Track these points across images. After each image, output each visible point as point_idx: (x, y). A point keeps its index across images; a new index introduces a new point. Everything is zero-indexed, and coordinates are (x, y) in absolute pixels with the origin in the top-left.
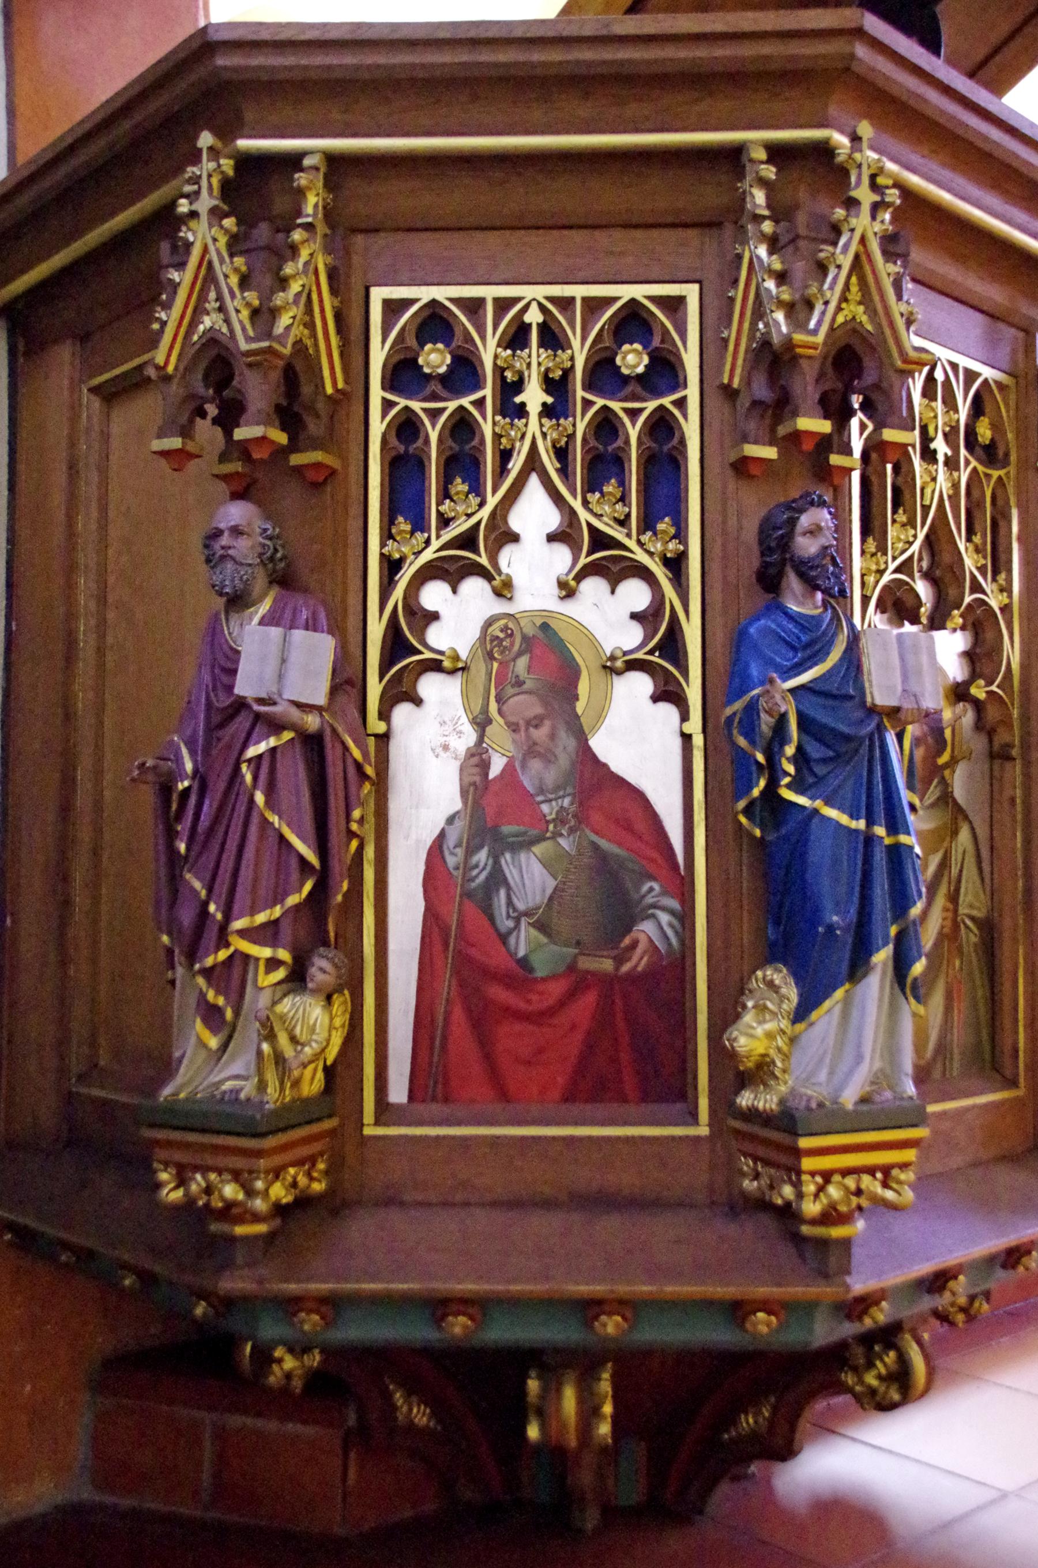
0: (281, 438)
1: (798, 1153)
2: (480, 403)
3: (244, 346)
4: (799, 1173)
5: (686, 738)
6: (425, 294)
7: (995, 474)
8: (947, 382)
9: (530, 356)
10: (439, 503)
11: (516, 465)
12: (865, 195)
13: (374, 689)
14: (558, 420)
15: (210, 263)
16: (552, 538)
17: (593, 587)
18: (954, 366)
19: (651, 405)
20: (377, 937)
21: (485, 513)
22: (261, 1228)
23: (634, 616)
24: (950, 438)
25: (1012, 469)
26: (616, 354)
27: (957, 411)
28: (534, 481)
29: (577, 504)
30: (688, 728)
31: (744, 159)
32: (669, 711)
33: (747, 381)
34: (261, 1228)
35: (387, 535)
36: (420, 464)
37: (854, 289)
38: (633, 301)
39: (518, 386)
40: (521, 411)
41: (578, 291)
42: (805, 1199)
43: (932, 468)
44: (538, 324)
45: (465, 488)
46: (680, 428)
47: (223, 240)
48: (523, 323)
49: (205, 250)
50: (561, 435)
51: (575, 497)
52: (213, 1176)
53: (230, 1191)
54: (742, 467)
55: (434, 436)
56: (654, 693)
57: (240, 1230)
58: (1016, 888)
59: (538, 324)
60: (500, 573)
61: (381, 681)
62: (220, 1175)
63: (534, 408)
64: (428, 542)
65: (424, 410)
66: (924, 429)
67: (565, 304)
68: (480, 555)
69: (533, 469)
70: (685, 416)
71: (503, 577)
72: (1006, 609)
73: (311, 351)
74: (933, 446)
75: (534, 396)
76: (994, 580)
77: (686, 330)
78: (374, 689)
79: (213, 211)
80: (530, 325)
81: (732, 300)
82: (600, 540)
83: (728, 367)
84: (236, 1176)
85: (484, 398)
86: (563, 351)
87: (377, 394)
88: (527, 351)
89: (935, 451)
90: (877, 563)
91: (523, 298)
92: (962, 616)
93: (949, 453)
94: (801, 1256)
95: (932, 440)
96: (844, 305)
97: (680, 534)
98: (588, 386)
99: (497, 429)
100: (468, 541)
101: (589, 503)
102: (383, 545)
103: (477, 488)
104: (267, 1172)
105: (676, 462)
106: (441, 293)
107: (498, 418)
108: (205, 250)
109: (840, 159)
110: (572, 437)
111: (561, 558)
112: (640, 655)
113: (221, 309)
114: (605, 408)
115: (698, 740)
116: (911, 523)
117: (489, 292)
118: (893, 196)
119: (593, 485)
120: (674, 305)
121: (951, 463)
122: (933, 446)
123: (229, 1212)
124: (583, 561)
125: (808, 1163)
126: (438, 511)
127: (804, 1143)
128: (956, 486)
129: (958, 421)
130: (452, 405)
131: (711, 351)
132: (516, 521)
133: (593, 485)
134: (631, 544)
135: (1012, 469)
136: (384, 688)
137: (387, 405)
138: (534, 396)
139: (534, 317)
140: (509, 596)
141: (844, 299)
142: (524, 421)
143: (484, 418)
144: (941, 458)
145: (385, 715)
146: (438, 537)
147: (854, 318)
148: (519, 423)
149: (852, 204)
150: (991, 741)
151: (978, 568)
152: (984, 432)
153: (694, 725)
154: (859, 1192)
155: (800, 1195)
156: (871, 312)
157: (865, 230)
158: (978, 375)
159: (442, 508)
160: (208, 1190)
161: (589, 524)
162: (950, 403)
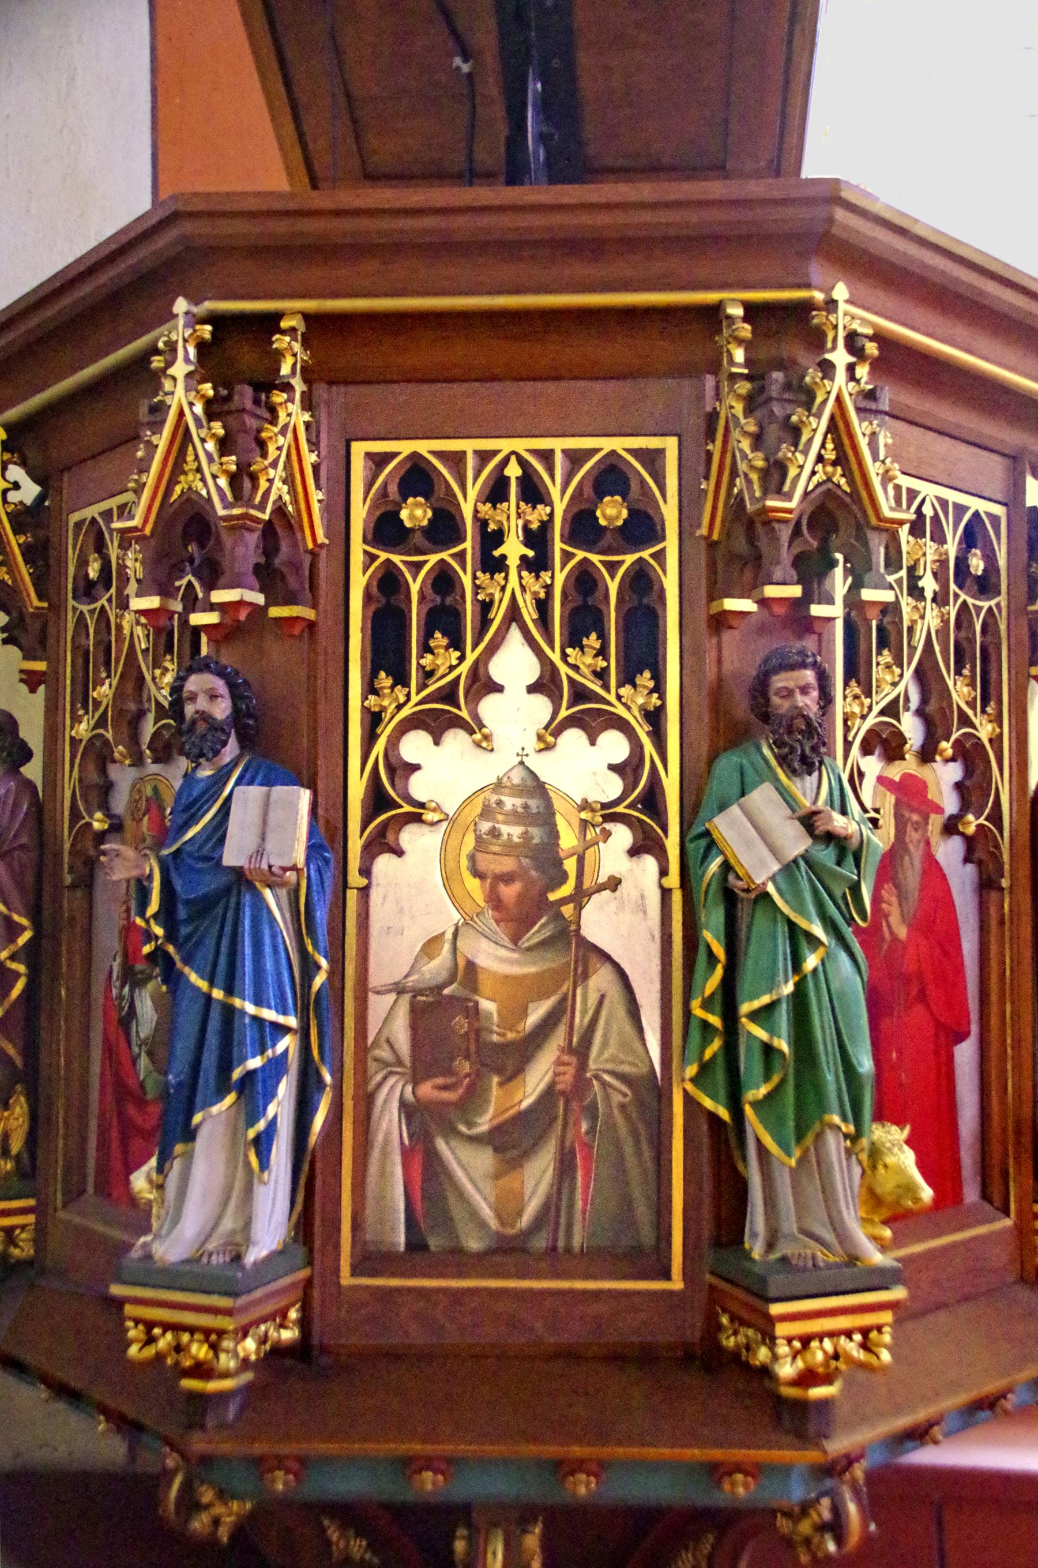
0: (259, 599)
2: (461, 557)
3: (221, 512)
5: (666, 893)
6: (405, 448)
7: (985, 605)
8: (936, 519)
10: (420, 656)
11: (498, 615)
12: (840, 357)
15: (187, 430)
16: (532, 689)
17: (574, 737)
18: (944, 503)
19: (629, 559)
21: (464, 669)
23: (612, 768)
25: (1002, 599)
29: (555, 657)
31: (722, 316)
33: (727, 534)
35: (370, 688)
38: (613, 453)
39: (498, 538)
41: (558, 445)
42: (781, 1361)
43: (921, 605)
44: (517, 478)
45: (445, 642)
46: (661, 582)
47: (199, 409)
49: (181, 414)
51: (553, 648)
53: (200, 1351)
54: (720, 622)
56: (632, 848)
58: (1012, 1003)
63: (513, 562)
65: (405, 563)
66: (912, 570)
72: (996, 741)
73: (290, 508)
74: (921, 584)
75: (513, 549)
76: (983, 711)
77: (665, 484)
78: (356, 844)
79: (189, 376)
81: (709, 455)
82: (580, 694)
89: (922, 589)
90: (862, 705)
91: (499, 451)
94: (779, 1417)
95: (920, 578)
97: (659, 688)
100: (449, 694)
102: (365, 698)
103: (456, 643)
106: (423, 447)
108: (181, 414)
109: (351, 1533)
110: (549, 588)
111: (541, 707)
112: (620, 809)
113: (199, 470)
114: (585, 560)
116: (899, 663)
117: (468, 446)
118: (872, 349)
120: (652, 459)
121: (940, 599)
122: (921, 584)
123: (202, 1370)
124: (564, 713)
125: (782, 1329)
126: (418, 664)
127: (776, 1309)
128: (946, 622)
130: (433, 559)
132: (498, 669)
133: (574, 639)
134: (612, 698)
135: (1002, 599)
138: (513, 549)
139: (513, 471)
140: (490, 748)
141: (820, 459)
142: (503, 575)
143: (465, 572)
144: (929, 594)
145: (366, 871)
148: (499, 577)
149: (827, 369)
150: (928, 1006)
151: (967, 703)
152: (977, 564)
154: (836, 1356)
157: (840, 389)
158: (967, 508)
159: (423, 662)
161: (569, 677)
162: (939, 538)
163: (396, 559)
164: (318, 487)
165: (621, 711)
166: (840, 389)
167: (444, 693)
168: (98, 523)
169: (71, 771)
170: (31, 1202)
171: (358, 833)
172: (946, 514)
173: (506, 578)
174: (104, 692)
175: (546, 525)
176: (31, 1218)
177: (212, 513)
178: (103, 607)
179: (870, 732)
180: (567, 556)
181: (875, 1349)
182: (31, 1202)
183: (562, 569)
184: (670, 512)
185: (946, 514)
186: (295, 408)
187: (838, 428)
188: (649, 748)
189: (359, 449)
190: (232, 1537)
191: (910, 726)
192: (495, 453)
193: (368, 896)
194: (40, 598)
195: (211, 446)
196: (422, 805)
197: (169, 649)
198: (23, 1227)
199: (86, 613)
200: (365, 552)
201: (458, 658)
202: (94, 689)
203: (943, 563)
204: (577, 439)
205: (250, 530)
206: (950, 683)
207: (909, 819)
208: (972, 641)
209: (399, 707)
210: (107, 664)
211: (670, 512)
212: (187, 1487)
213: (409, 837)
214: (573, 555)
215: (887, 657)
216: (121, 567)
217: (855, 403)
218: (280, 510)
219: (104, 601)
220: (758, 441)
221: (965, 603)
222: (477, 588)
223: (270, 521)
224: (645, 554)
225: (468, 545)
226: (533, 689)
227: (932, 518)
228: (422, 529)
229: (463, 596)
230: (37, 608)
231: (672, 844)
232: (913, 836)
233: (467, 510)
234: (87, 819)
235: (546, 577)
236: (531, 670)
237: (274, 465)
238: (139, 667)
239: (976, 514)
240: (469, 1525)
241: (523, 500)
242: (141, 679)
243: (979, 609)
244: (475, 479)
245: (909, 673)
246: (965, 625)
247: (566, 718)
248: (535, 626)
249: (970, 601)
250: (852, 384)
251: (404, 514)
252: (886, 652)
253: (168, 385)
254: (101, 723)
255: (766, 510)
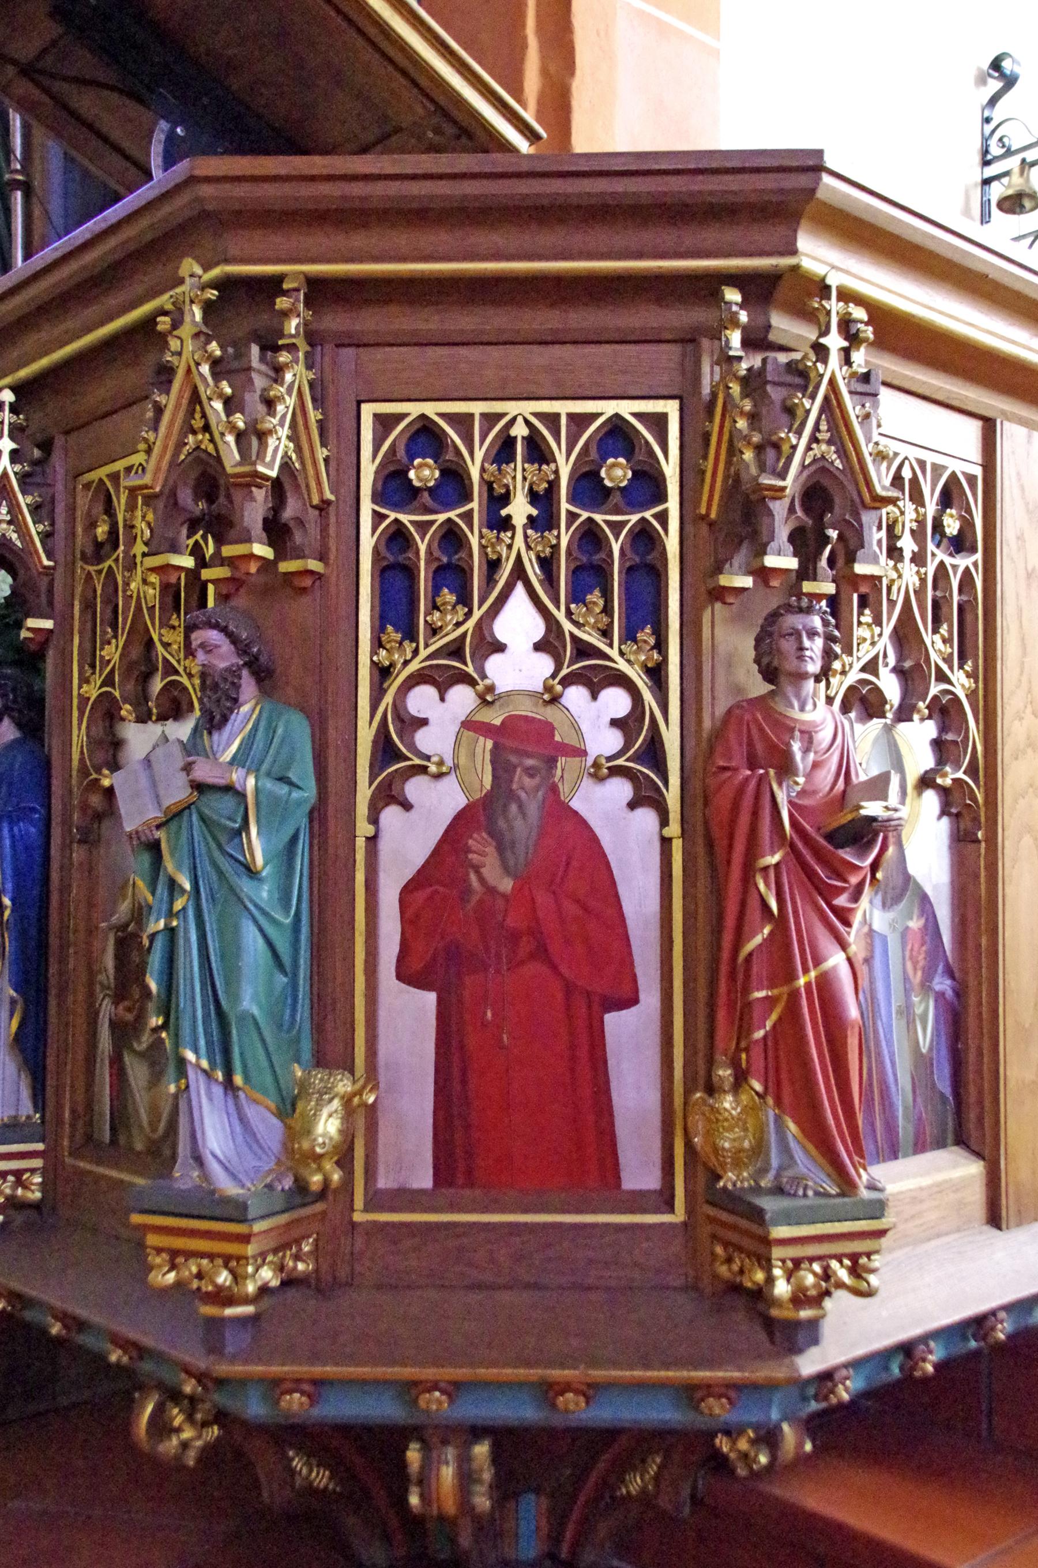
1: (767, 1242)
2: (468, 516)
4: (769, 1260)
5: (666, 842)
8: (915, 481)
9: (515, 470)
13: (364, 792)
14: (542, 533)
18: (922, 464)
20: (367, 1041)
21: (470, 624)
22: (249, 1309)
24: (918, 535)
26: (601, 467)
27: (923, 505)
28: (520, 589)
29: (560, 616)
30: (667, 832)
32: (646, 818)
34: (249, 1309)
35: (378, 644)
36: (410, 573)
37: (824, 427)
39: (505, 499)
40: (505, 524)
41: (563, 408)
44: (523, 438)
48: (509, 436)
50: (541, 480)
51: (558, 608)
52: (205, 1262)
53: (223, 1278)
55: (423, 548)
57: (229, 1312)
59: (523, 438)
60: (484, 676)
61: (370, 785)
62: (212, 1261)
64: (416, 652)
67: (552, 420)
68: (465, 664)
69: (518, 579)
70: (666, 530)
71: (487, 682)
73: (297, 465)
74: (899, 544)
75: (520, 509)
78: (364, 792)
80: (516, 437)
82: (583, 650)
83: (705, 497)
84: (227, 1260)
85: (472, 510)
86: (548, 464)
87: (367, 508)
88: (512, 465)
89: (901, 549)
92: (928, 707)
93: (916, 549)
95: (899, 538)
96: (814, 446)
97: (661, 645)
98: (572, 499)
99: (483, 541)
100: (455, 650)
101: (572, 614)
102: (374, 652)
103: (464, 599)
104: (255, 1257)
105: (657, 574)
107: (485, 531)
110: (556, 548)
112: (621, 762)
114: (590, 520)
115: (677, 846)
116: (878, 621)
117: (477, 408)
119: (577, 596)
121: (919, 559)
123: (223, 1297)
125: (777, 1252)
126: (426, 621)
128: (923, 581)
129: (925, 515)
130: (441, 517)
131: (690, 475)
132: (503, 628)
134: (614, 653)
136: (373, 793)
137: (378, 517)
138: (520, 509)
139: (520, 431)
141: (814, 439)
142: (509, 534)
143: (472, 533)
144: (907, 555)
145: (374, 819)
146: (427, 646)
147: (823, 457)
148: (506, 536)
153: (674, 829)
155: (770, 1280)
156: (842, 453)
158: (945, 468)
160: (200, 1276)
162: (917, 498)
163: (404, 518)
164: (324, 444)
165: (622, 665)
166: (833, 374)
167: (452, 648)
168: (105, 484)
169: (80, 729)
170: (40, 1146)
171: (367, 784)
172: (924, 472)
173: (512, 538)
174: (112, 652)
175: (553, 485)
176: (37, 1163)
177: (219, 469)
178: (110, 567)
179: (851, 689)
180: (572, 516)
181: (864, 1275)
182: (40, 1146)
183: (568, 529)
184: (671, 470)
185: (924, 472)
186: (300, 368)
187: (832, 406)
188: (648, 696)
189: (368, 411)
190: (199, 1460)
191: (890, 687)
192: (502, 416)
193: (375, 845)
194: (49, 558)
195: (218, 405)
196: (428, 758)
197: (177, 608)
198: (33, 1171)
199: (93, 573)
200: (374, 511)
201: (465, 614)
202: (102, 649)
203: (921, 522)
204: (678, 703)
205: (260, 487)
206: (928, 641)
207: (520, 764)
208: (949, 601)
209: (406, 663)
210: (114, 626)
211: (671, 470)
212: (160, 1410)
213: (415, 788)
214: (578, 516)
215: (867, 617)
216: (130, 527)
217: (848, 385)
218: (286, 466)
219: (110, 562)
220: (753, 418)
221: (942, 564)
222: (483, 547)
223: (278, 478)
224: (648, 514)
225: (474, 505)
226: (538, 647)
227: (910, 480)
228: (430, 490)
229: (471, 556)
230: (45, 567)
231: (673, 796)
232: (522, 782)
233: (475, 473)
234: (94, 776)
235: (551, 537)
236: (537, 629)
237: (282, 424)
238: (146, 623)
239: (953, 475)
240: (422, 1440)
241: (528, 462)
242: (150, 642)
243: (955, 567)
244: (482, 442)
245: (888, 629)
246: (941, 584)
247: (567, 675)
248: (541, 585)
249: (948, 561)
250: (845, 368)
251: (412, 474)
252: (867, 611)
253: (174, 344)
254: (109, 681)
255: (761, 488)
